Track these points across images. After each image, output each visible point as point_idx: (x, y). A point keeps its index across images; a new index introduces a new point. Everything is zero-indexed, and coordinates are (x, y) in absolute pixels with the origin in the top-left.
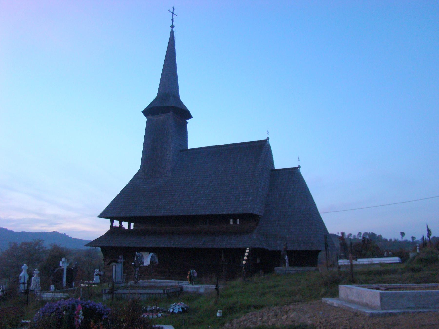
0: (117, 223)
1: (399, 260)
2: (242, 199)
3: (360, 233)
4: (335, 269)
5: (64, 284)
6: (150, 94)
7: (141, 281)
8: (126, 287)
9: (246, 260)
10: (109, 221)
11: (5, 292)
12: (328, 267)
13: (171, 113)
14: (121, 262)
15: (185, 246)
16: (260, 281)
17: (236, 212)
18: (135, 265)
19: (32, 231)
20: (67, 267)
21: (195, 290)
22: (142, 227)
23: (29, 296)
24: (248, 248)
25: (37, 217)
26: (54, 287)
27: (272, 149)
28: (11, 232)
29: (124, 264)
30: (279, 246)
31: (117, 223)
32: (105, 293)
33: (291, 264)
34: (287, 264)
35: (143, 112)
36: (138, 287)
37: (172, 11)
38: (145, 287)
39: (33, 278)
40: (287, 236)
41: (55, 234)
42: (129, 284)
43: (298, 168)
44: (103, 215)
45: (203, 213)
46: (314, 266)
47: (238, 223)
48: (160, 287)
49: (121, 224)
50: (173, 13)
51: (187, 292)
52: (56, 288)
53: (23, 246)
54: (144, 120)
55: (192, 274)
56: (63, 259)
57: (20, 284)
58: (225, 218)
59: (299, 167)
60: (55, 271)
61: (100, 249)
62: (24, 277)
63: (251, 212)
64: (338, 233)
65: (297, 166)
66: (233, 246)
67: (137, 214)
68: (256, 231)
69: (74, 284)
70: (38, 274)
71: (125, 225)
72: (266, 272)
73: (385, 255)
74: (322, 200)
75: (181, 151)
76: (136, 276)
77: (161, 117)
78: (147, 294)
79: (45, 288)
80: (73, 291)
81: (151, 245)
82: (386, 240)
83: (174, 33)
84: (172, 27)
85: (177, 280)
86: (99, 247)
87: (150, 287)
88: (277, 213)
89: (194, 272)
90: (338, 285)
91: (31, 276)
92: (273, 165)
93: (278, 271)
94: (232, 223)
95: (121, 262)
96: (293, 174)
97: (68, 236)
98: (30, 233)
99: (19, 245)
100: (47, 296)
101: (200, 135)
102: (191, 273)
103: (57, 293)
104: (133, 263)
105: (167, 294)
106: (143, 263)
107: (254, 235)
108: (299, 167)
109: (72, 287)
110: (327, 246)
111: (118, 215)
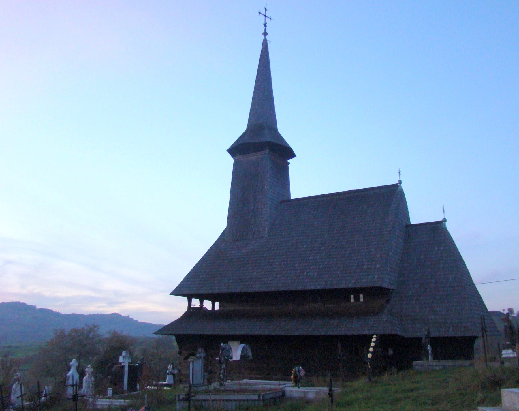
0: (196, 302)
2: (366, 267)
4: (496, 365)
5: (126, 387)
6: (238, 126)
7: (228, 383)
8: (207, 392)
9: (372, 353)
10: (185, 299)
11: (48, 397)
12: (486, 361)
13: (267, 151)
14: (201, 357)
15: (289, 333)
16: (393, 382)
17: (358, 285)
18: (220, 361)
19: (86, 313)
20: (129, 363)
21: (303, 395)
22: (231, 307)
23: (79, 404)
24: (375, 336)
25: (93, 294)
26: (111, 391)
27: (406, 196)
28: (57, 314)
29: (206, 359)
31: (196, 302)
32: (179, 400)
33: (435, 357)
34: (430, 357)
35: (227, 150)
36: (224, 391)
37: (263, 12)
38: (234, 391)
39: (85, 378)
41: (115, 317)
42: (212, 387)
44: (177, 292)
46: (469, 359)
47: (362, 300)
48: (254, 391)
49: (201, 303)
50: (265, 16)
51: (291, 398)
52: (114, 393)
53: (73, 334)
54: (230, 161)
55: (298, 373)
56: (124, 353)
57: (67, 386)
58: (343, 294)
59: (445, 220)
60: (113, 369)
61: (174, 338)
62: (73, 377)
63: (379, 285)
64: (504, 310)
66: (356, 333)
67: (224, 290)
68: (386, 311)
69: (138, 387)
70: (92, 373)
71: (208, 304)
72: (400, 369)
74: (477, 265)
75: (282, 202)
76: (221, 376)
77: (253, 157)
78: (235, 400)
79: (99, 390)
80: (137, 397)
81: (242, 333)
83: (268, 42)
84: (265, 34)
85: (277, 380)
86: (172, 335)
87: (241, 391)
88: (415, 286)
89: (300, 370)
90: (500, 389)
91: (82, 374)
93: (417, 367)
94: (352, 300)
95: (201, 357)
96: (437, 230)
97: (132, 319)
98: (82, 315)
99: (67, 333)
100: (102, 402)
101: (306, 180)
102: (295, 371)
103: (115, 398)
104: (217, 358)
105: (263, 400)
106: (232, 358)
108: (445, 220)
109: (136, 390)
110: (486, 331)
111: (196, 292)
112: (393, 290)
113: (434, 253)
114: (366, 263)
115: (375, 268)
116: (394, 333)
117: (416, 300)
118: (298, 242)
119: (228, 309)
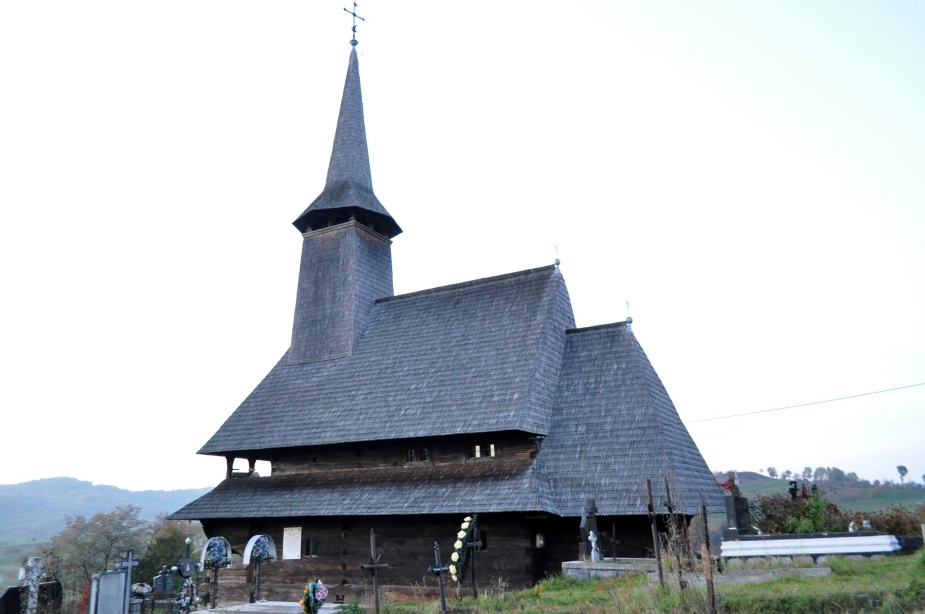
0: (241, 465)
1: (892, 544)
3: (808, 470)
10: (223, 460)
13: (352, 222)
17: (484, 429)
22: (290, 471)
24: (468, 519)
27: (567, 284)
30: (573, 505)
31: (241, 465)
34: (593, 553)
37: (351, 8)
40: (603, 481)
43: (625, 323)
44: (208, 450)
45: (412, 435)
47: (493, 454)
49: (252, 465)
54: (297, 238)
58: (461, 444)
65: (624, 320)
67: (276, 442)
68: (530, 471)
73: (851, 530)
75: (377, 301)
77: (332, 232)
82: (866, 484)
84: (354, 43)
88: (580, 429)
92: (572, 320)
94: (478, 454)
96: (615, 335)
101: (414, 268)
107: (525, 480)
112: (541, 435)
113: (612, 373)
114: (498, 393)
115: (511, 399)
116: (539, 509)
117: (580, 452)
118: (395, 363)
119: (288, 473)
